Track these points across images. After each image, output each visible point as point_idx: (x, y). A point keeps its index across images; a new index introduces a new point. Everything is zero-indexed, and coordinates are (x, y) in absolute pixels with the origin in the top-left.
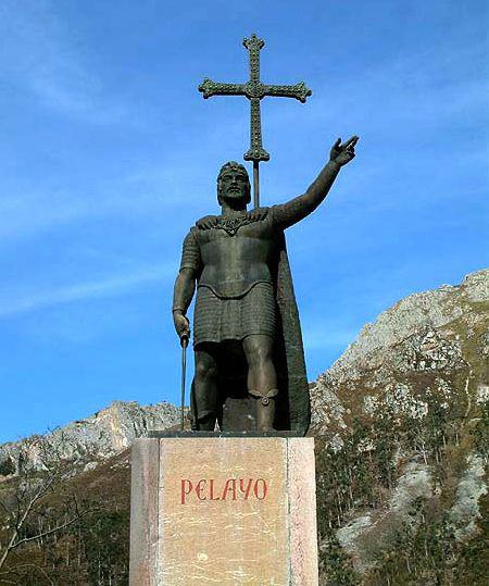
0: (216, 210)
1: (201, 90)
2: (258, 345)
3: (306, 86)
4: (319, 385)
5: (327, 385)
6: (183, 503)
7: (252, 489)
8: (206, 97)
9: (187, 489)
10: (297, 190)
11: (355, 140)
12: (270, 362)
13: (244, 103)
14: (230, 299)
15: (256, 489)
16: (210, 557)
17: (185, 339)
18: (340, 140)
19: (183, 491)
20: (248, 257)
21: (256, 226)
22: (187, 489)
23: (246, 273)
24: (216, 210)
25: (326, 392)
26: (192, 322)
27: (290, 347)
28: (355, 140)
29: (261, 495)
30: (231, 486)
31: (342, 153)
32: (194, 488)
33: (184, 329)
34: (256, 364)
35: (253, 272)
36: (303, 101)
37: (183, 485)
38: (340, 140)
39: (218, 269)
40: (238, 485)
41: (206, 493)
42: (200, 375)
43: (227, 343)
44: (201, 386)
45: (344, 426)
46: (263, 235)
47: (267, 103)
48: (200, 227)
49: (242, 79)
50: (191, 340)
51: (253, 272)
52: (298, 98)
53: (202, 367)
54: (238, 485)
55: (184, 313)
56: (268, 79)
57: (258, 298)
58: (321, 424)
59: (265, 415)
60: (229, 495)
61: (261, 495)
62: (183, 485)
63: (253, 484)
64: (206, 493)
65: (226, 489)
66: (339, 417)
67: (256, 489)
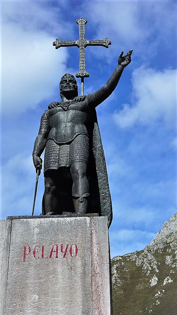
0: (58, 100)
1: (54, 45)
2: (79, 167)
4: (146, 251)
5: (149, 251)
7: (68, 252)
8: (57, 48)
9: (27, 252)
11: (131, 52)
12: (85, 177)
14: (63, 144)
17: (38, 169)
18: (123, 53)
20: (74, 121)
21: (80, 104)
23: (73, 127)
25: (149, 254)
26: (43, 160)
27: (100, 174)
28: (131, 52)
33: (38, 164)
34: (77, 178)
35: (77, 128)
36: (107, 47)
38: (123, 53)
39: (57, 129)
42: (47, 190)
43: (61, 169)
44: (48, 196)
45: (158, 271)
46: (83, 109)
48: (49, 108)
50: (42, 171)
51: (77, 128)
52: (104, 46)
53: (48, 185)
55: (39, 155)
57: (79, 142)
58: (147, 270)
59: (81, 206)
60: (54, 254)
63: (69, 247)
65: (52, 252)
66: (155, 267)
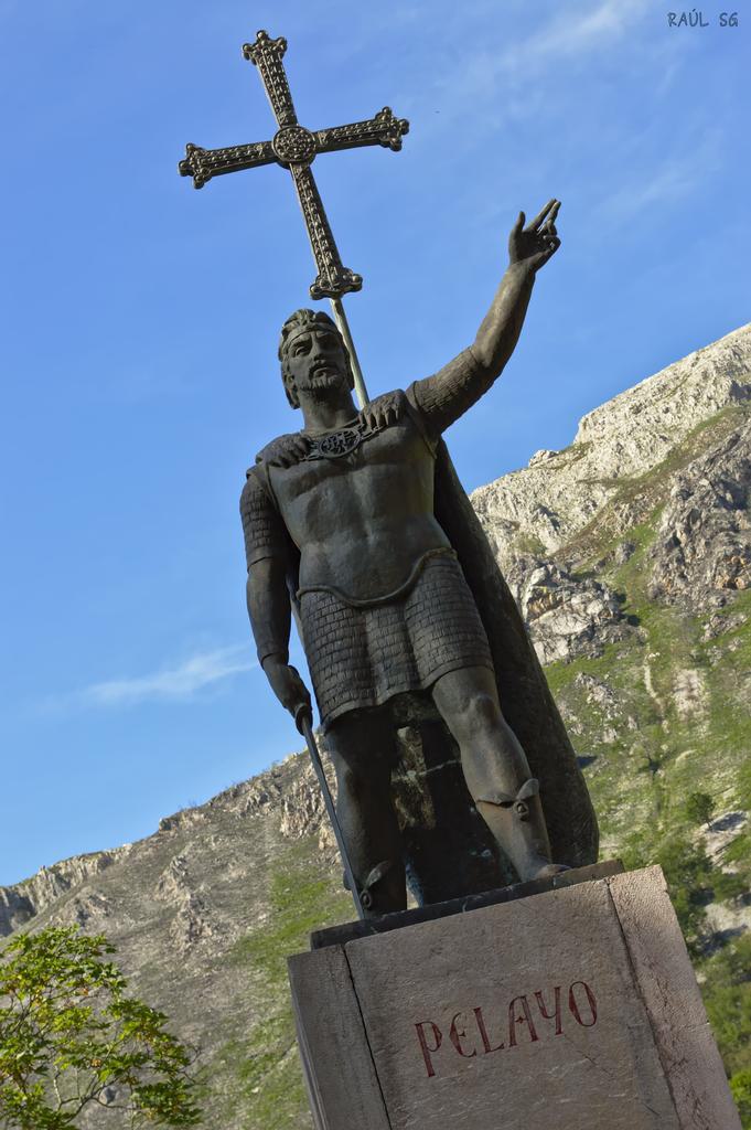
0: (294, 422)
3: (394, 114)
6: (431, 1074)
7: (566, 1012)
8: (199, 186)
9: (431, 1041)
10: (467, 338)
11: (553, 209)
13: (278, 181)
15: (573, 1006)
16: (13, 915)
18: (523, 217)
19: (423, 1044)
22: (431, 1041)
24: (294, 422)
28: (553, 209)
29: (586, 1017)
30: (519, 1010)
31: (533, 244)
32: (446, 1037)
37: (421, 1034)
38: (523, 217)
40: (534, 1004)
41: (473, 1040)
47: (322, 165)
49: (264, 127)
52: (386, 145)
54: (534, 1004)
56: (314, 119)
60: (522, 1032)
61: (586, 1017)
62: (421, 1034)
63: (565, 996)
64: (473, 1040)
67: (573, 1006)
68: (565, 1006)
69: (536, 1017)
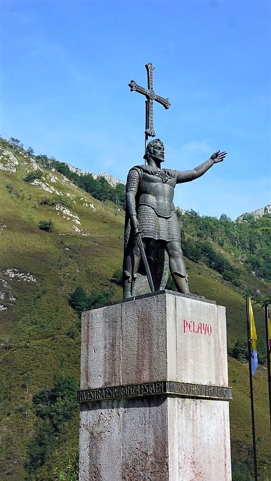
9: (186, 325)
30: (200, 326)
41: (192, 328)
60: (200, 329)
64: (192, 328)
68: (207, 328)
69: (202, 328)
